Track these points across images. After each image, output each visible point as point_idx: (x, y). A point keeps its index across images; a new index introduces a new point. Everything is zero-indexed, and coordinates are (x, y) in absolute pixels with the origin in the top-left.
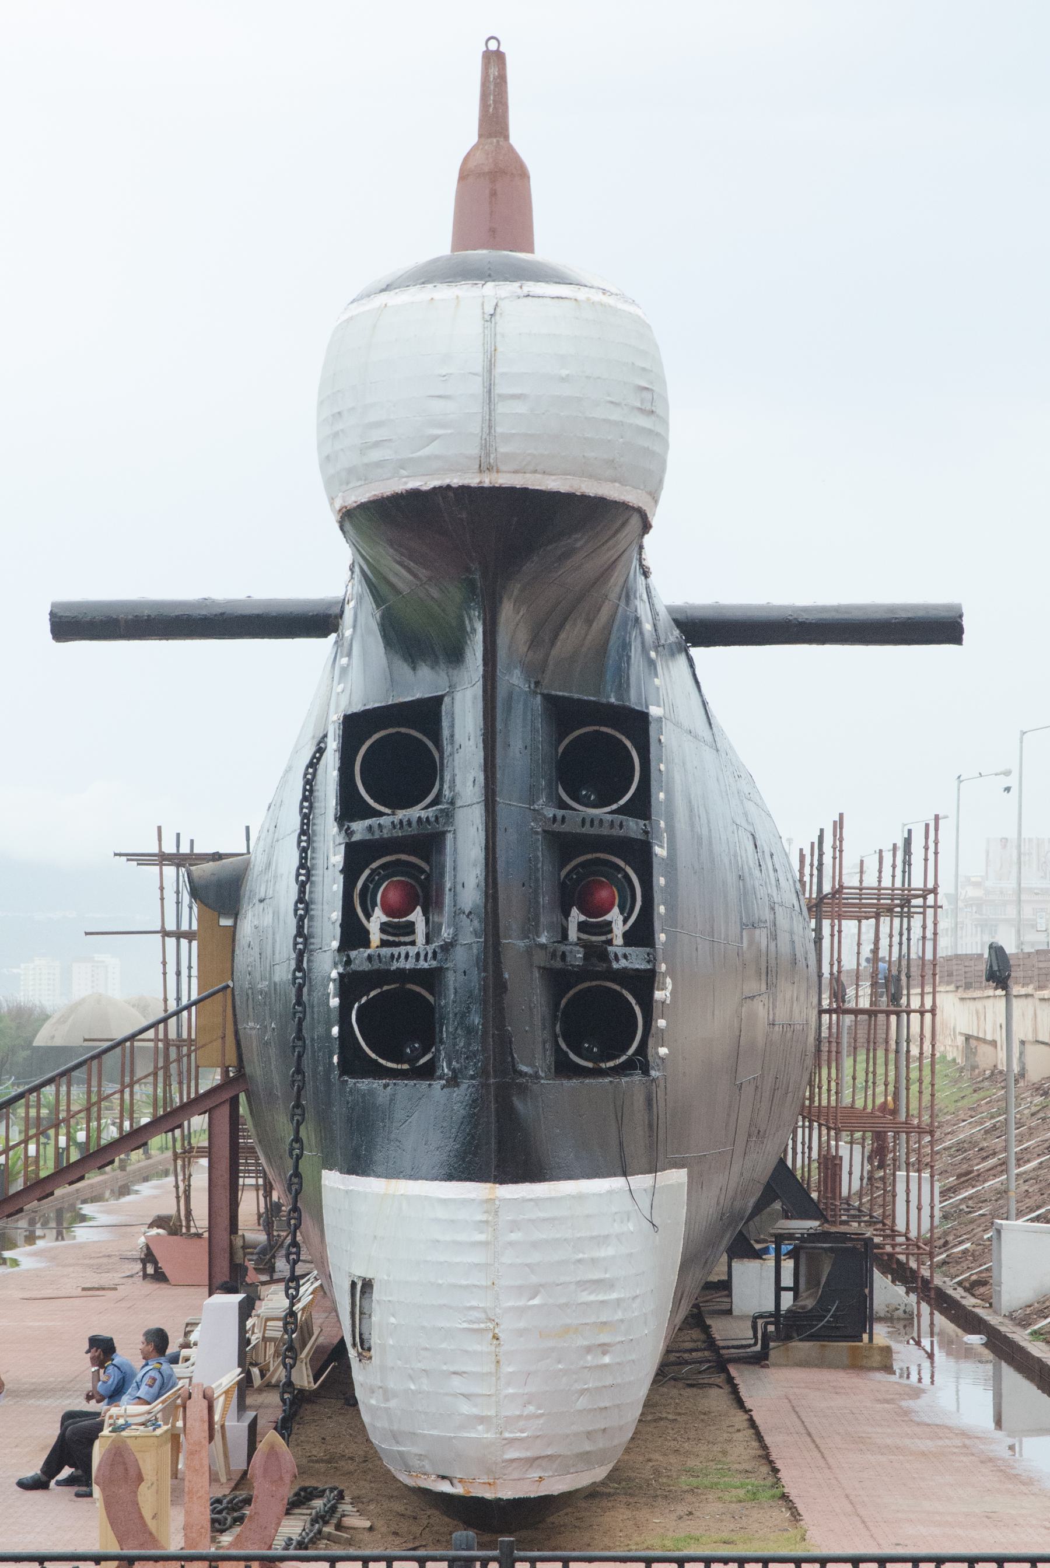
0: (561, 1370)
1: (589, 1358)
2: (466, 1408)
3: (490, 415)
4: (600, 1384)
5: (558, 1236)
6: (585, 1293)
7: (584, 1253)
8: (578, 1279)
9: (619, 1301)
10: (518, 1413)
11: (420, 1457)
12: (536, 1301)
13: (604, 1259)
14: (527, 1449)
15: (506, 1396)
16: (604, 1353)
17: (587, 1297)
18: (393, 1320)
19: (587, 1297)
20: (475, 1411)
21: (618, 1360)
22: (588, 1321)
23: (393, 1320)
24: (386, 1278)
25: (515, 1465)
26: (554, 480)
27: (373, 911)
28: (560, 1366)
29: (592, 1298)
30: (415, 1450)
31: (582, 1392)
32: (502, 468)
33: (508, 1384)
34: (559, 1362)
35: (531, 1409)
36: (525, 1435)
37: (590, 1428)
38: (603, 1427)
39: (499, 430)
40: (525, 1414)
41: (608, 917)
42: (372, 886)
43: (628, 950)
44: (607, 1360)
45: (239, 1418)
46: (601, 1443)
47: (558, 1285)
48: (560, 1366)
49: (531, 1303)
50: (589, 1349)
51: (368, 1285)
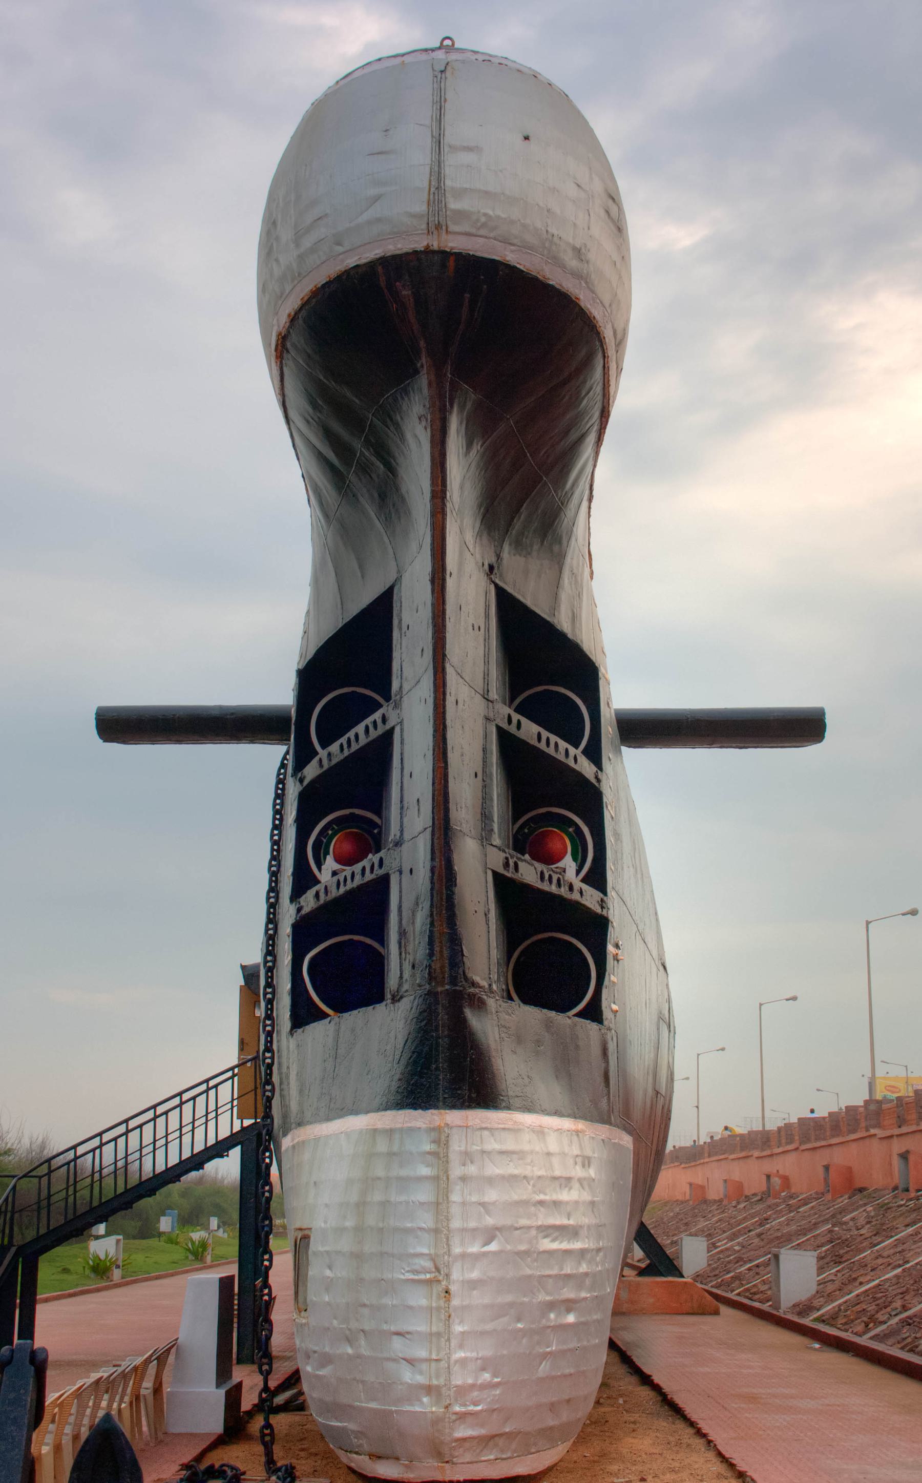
0: (521, 1330)
1: (552, 1316)
2: (408, 1376)
3: (439, 166)
4: (565, 1347)
5: (516, 1172)
6: (546, 1241)
7: (545, 1194)
8: (540, 1223)
9: (583, 1252)
10: (470, 1381)
11: (359, 1434)
12: (493, 1247)
13: (567, 1203)
14: (482, 1426)
15: (456, 1362)
16: (569, 1311)
17: (547, 1244)
18: (328, 1273)
19: (547, 1244)
20: (421, 1379)
21: (583, 1319)
22: (551, 1273)
23: (328, 1273)
24: (323, 1225)
25: (467, 1445)
26: (512, 251)
27: (325, 859)
28: (520, 1325)
29: (555, 1246)
30: (352, 1426)
31: (545, 1356)
32: (453, 228)
33: (461, 1346)
34: (519, 1320)
35: (487, 1376)
36: (479, 1408)
37: (554, 1399)
38: (567, 1398)
39: (448, 183)
40: (479, 1382)
41: (561, 864)
42: (325, 841)
43: (585, 887)
44: (571, 1318)
45: (219, 1385)
46: (565, 1416)
47: (517, 1229)
48: (520, 1325)
49: (486, 1249)
50: (551, 1306)
51: (306, 1238)
